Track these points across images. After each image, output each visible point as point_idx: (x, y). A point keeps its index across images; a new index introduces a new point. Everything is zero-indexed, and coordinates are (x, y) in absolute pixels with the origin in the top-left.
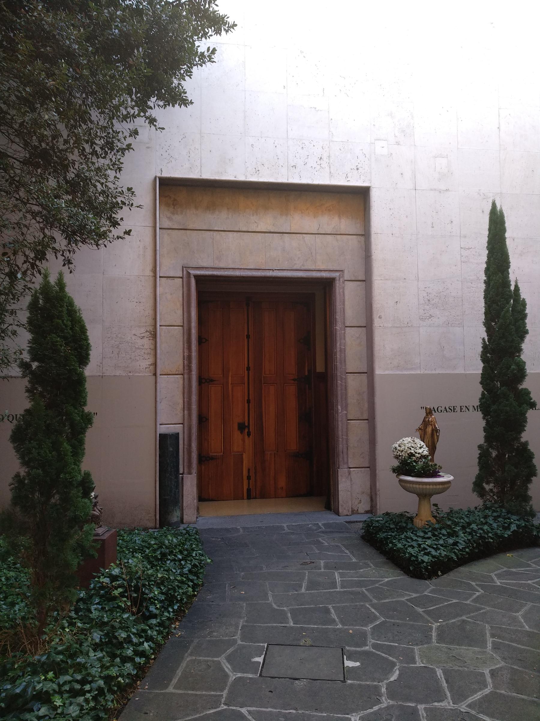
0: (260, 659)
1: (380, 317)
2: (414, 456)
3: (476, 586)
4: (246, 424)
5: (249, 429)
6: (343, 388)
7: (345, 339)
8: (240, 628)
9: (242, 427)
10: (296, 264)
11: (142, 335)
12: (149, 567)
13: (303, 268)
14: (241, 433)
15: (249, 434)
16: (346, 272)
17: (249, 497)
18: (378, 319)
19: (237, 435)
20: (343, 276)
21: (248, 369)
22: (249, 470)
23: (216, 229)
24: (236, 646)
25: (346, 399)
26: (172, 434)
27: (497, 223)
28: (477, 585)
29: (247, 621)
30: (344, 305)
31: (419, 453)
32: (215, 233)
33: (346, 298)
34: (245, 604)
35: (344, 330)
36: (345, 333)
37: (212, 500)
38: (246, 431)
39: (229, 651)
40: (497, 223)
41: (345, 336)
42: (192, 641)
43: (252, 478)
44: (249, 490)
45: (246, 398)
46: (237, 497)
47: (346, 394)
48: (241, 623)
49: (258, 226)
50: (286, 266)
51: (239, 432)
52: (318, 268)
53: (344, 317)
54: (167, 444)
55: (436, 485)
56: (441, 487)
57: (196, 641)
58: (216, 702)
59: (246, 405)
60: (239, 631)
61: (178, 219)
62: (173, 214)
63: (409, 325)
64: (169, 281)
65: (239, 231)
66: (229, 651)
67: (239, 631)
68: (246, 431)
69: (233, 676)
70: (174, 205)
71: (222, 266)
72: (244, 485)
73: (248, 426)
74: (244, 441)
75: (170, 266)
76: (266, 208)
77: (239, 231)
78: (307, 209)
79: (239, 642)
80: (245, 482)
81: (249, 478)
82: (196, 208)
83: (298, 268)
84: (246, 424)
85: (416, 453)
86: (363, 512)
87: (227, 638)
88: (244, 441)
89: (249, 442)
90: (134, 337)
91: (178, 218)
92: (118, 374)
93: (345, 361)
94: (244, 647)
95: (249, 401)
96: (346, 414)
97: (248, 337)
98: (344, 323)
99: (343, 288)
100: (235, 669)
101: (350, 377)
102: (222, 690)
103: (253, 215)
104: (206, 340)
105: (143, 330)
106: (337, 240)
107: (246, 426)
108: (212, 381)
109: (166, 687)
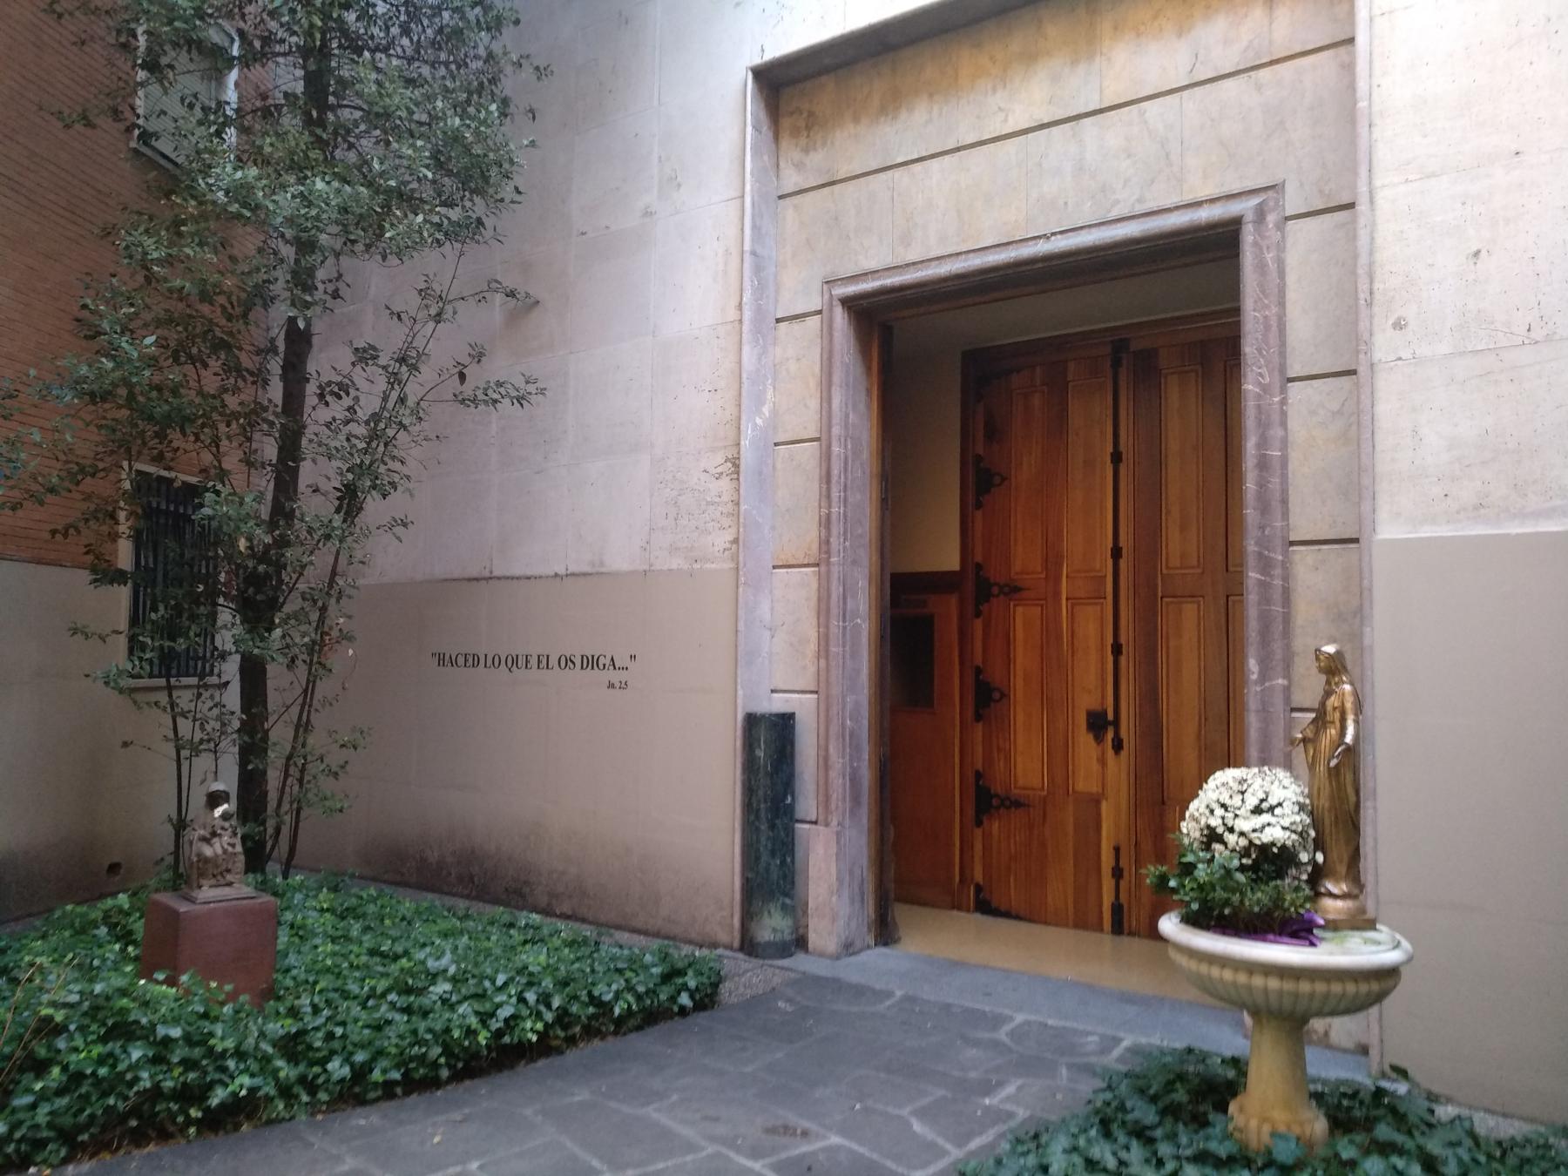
1: (1399, 325)
2: (1220, 839)
4: (1110, 716)
5: (1117, 733)
6: (1277, 595)
7: (1284, 424)
9: (1098, 723)
10: (1117, 202)
11: (719, 470)
13: (1140, 209)
14: (1099, 739)
15: (1118, 746)
16: (1290, 189)
17: (1118, 928)
18: (1390, 332)
19: (1085, 741)
20: (1279, 205)
21: (1116, 553)
22: (1117, 850)
23: (900, 160)
25: (1287, 633)
26: (763, 716)
30: (1282, 304)
31: (1242, 834)
32: (897, 173)
33: (1291, 279)
35: (1283, 390)
36: (1284, 402)
37: (1018, 917)
38: (1110, 735)
41: (1284, 414)
43: (1126, 874)
44: (1117, 909)
45: (1110, 640)
46: (1083, 921)
47: (1287, 619)
49: (1006, 120)
50: (1086, 215)
51: (1091, 736)
52: (1188, 197)
53: (1283, 344)
54: (769, 744)
55: (1312, 980)
56: (1351, 988)
59: (1110, 658)
61: (819, 162)
62: (806, 151)
63: (1537, 334)
64: (796, 326)
65: (958, 149)
68: (1110, 735)
70: (808, 128)
71: (912, 256)
72: (1105, 888)
73: (1116, 723)
74: (1102, 762)
75: (801, 290)
76: (1030, 58)
77: (958, 149)
78: (1155, 17)
80: (1108, 884)
81: (1117, 873)
82: (856, 120)
83: (1126, 212)
84: (1110, 716)
85: (1231, 830)
86: (1350, 1044)
88: (1102, 762)
89: (1119, 770)
90: (704, 477)
91: (817, 158)
92: (674, 566)
93: (1285, 502)
95: (1117, 650)
96: (1287, 690)
97: (1117, 458)
98: (1282, 368)
99: (1281, 247)
101: (1304, 559)
103: (994, 90)
104: (1004, 479)
105: (720, 458)
106: (1259, 87)
107: (1110, 723)
108: (1017, 589)
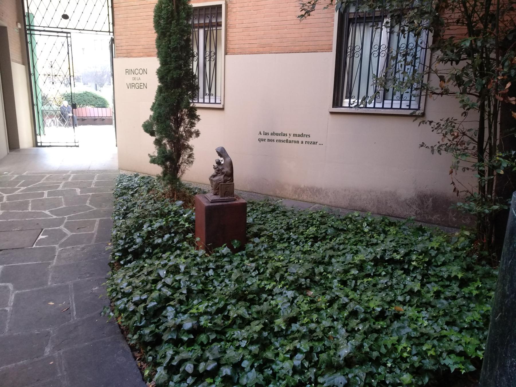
0: (41, 237)
3: (93, 207)
8: (56, 257)
12: (273, 348)
24: (60, 243)
27: (419, 125)
28: (92, 209)
29: (49, 264)
34: (49, 283)
39: (65, 239)
40: (419, 125)
42: (96, 242)
48: (55, 262)
57: (93, 242)
58: (69, 218)
60: (57, 254)
65: (50, 146)
66: (65, 239)
67: (57, 254)
69: (62, 227)
79: (57, 246)
87: (68, 247)
94: (53, 243)
100: (60, 230)
102: (67, 222)
109: (100, 220)
